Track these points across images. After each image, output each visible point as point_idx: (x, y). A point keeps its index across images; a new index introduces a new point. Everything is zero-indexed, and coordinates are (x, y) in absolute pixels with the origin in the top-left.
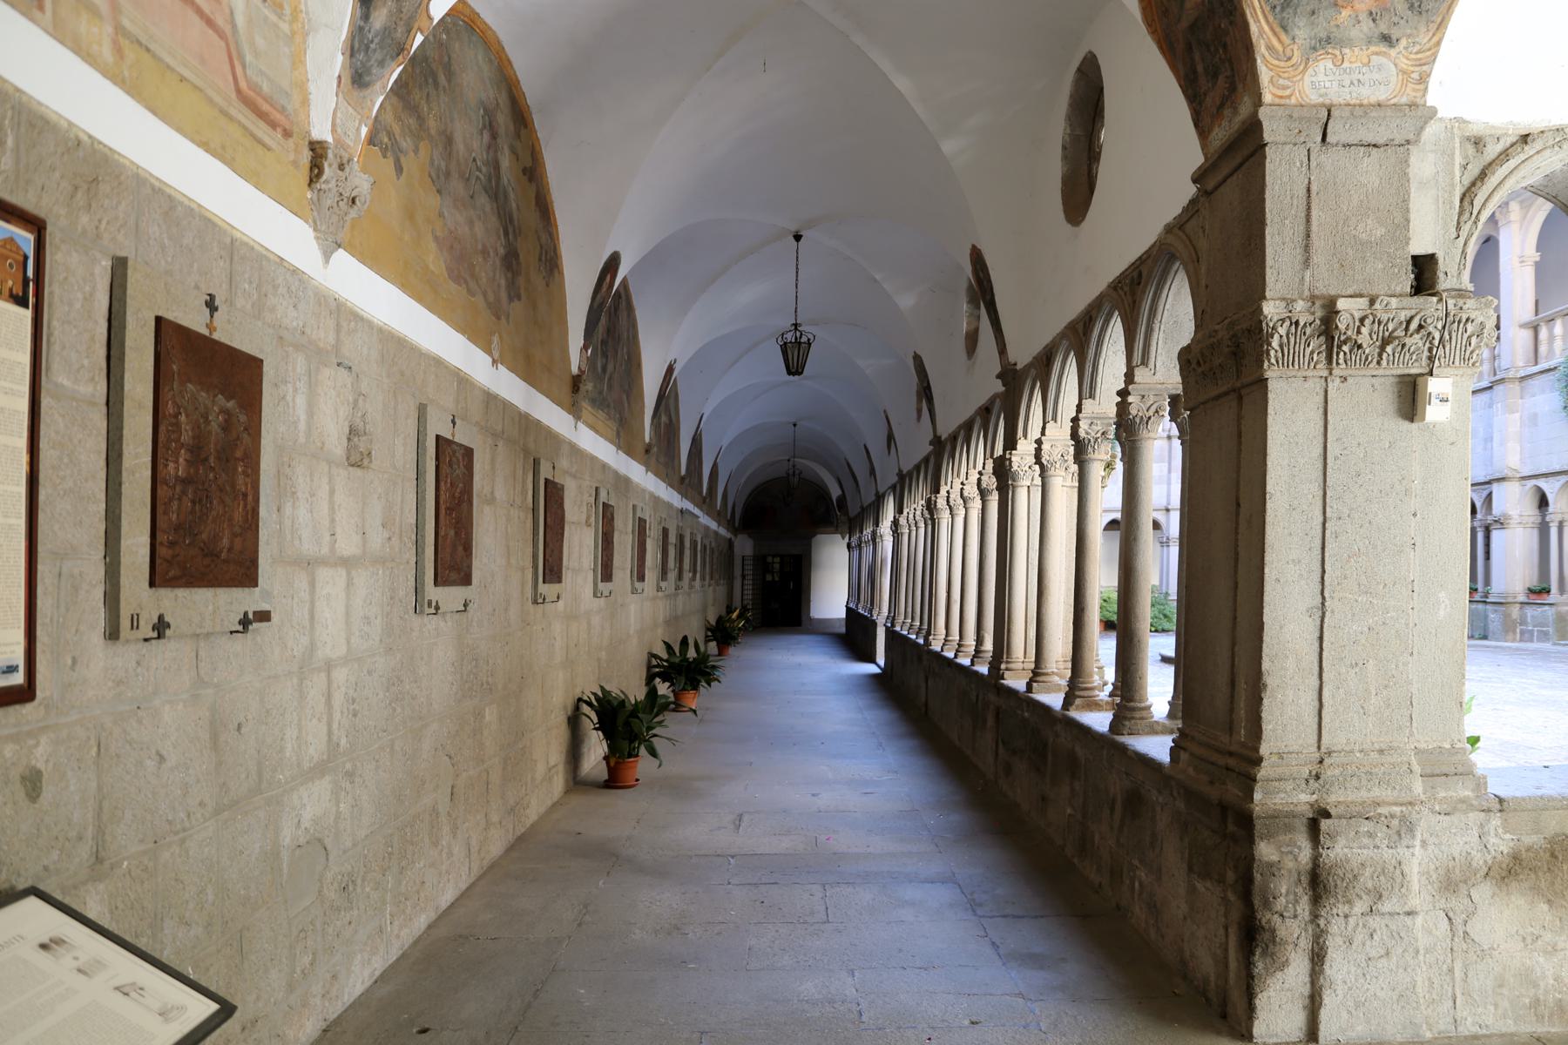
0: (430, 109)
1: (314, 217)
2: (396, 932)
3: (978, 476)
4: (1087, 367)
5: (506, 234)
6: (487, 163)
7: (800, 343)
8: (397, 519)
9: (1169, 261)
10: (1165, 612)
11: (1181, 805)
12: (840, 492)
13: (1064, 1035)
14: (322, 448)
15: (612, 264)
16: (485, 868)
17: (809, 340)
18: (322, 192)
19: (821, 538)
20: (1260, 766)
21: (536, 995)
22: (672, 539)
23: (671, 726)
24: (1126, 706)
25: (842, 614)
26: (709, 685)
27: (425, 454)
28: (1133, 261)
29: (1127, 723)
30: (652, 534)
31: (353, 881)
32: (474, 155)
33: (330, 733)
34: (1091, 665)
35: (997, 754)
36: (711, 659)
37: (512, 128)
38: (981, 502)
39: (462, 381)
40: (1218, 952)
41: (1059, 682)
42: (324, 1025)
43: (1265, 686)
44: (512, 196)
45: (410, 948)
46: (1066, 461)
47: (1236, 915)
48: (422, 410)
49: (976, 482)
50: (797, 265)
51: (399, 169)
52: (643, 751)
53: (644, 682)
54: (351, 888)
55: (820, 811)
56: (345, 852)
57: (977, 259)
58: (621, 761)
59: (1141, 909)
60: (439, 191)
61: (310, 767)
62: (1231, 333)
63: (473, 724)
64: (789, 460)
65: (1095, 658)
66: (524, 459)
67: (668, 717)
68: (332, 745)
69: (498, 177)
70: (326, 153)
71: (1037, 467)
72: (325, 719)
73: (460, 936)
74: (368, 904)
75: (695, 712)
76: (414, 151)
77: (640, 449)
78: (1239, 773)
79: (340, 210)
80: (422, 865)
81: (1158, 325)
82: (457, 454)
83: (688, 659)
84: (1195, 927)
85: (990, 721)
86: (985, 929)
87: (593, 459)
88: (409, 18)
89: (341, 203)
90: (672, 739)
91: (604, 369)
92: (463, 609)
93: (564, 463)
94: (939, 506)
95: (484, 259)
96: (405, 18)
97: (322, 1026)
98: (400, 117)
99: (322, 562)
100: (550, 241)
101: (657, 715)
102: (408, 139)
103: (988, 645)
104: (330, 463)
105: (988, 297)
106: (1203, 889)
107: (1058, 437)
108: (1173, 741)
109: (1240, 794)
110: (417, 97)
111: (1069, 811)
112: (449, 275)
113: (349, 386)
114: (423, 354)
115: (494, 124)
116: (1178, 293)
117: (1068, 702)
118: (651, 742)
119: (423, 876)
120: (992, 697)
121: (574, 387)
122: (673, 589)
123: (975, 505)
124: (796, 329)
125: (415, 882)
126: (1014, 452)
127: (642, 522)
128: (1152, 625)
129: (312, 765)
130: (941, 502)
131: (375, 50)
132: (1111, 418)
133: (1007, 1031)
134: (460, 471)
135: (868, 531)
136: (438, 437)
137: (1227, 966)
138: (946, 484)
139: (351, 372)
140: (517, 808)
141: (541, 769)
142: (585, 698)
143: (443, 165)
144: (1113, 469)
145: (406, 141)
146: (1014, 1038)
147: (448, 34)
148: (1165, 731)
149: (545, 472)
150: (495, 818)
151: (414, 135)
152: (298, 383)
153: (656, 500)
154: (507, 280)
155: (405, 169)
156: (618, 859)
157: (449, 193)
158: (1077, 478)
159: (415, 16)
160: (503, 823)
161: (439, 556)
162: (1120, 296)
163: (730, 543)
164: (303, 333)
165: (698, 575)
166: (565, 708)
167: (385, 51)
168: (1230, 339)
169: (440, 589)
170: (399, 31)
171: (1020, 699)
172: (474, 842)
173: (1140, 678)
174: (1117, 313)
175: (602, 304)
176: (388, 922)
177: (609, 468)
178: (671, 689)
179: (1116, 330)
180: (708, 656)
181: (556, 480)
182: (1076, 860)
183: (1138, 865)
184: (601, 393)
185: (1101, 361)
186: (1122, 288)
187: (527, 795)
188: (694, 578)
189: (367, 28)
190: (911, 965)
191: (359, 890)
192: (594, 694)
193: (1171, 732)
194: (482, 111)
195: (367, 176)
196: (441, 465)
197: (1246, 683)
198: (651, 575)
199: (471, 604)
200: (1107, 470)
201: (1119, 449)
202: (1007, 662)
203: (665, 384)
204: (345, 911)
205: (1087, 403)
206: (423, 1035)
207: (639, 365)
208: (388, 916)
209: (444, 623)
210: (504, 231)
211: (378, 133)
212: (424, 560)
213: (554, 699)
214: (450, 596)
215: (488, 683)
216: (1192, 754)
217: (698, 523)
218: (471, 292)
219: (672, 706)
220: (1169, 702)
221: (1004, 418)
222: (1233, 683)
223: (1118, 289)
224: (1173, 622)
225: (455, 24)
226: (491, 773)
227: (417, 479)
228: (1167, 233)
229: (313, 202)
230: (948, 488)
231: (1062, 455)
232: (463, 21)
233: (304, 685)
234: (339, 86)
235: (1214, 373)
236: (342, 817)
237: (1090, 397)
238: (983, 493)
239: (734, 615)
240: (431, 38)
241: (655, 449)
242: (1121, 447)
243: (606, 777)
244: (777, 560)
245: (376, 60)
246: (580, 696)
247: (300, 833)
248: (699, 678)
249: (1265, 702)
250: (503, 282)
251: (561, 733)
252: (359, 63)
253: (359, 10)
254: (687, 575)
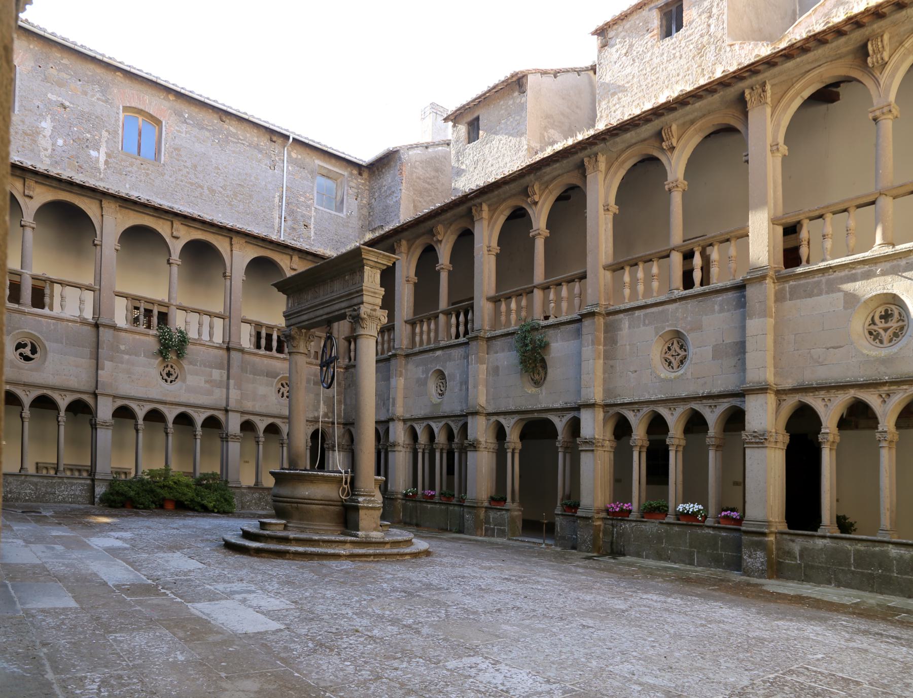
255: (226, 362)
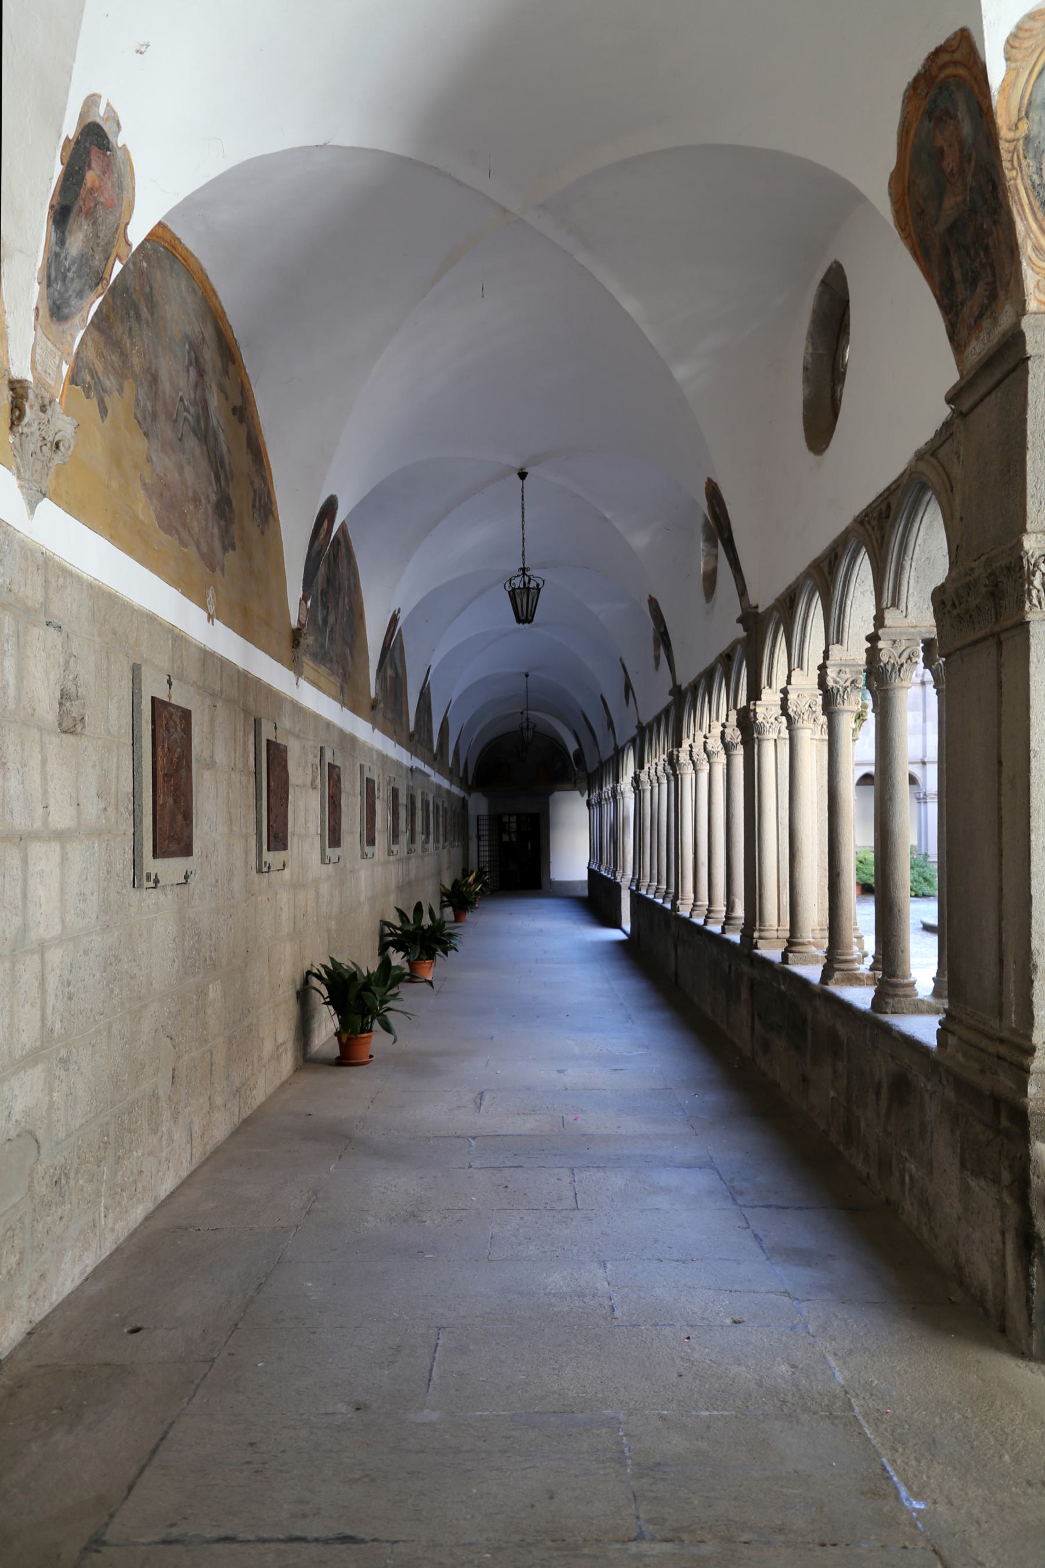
0: (133, 344)
1: (17, 464)
2: (110, 1226)
3: (722, 729)
4: (833, 609)
5: (218, 478)
6: (194, 403)
7: (529, 589)
8: (113, 789)
9: (920, 491)
10: (925, 875)
11: (950, 1094)
12: (577, 747)
13: (834, 1340)
14: (33, 715)
15: (329, 509)
16: (208, 1154)
17: (538, 585)
18: (24, 437)
19: (558, 795)
20: (1033, 1056)
21: (259, 1288)
22: (403, 799)
23: (407, 996)
24: (887, 982)
25: (584, 876)
26: (446, 954)
27: (140, 718)
28: (880, 492)
29: (890, 1000)
30: (381, 795)
31: (65, 1174)
32: (181, 394)
33: (43, 1018)
34: (849, 936)
35: (753, 1029)
36: (447, 925)
37: (219, 364)
38: (725, 756)
39: (177, 638)
40: (995, 1259)
41: (816, 953)
42: (28, 1327)
43: (1035, 967)
44: (222, 438)
45: (125, 1241)
46: (814, 712)
47: (1012, 1220)
48: (136, 671)
49: (720, 735)
50: (523, 505)
51: (103, 410)
52: (376, 1026)
53: (377, 952)
54: (63, 1181)
55: (566, 1089)
56: (58, 1144)
57: (713, 494)
58: (353, 1036)
59: (912, 1204)
60: (146, 434)
61: (22, 1056)
62: (989, 571)
63: (195, 1002)
64: (522, 713)
65: (853, 927)
66: (244, 720)
67: (403, 989)
68: (46, 1032)
69: (207, 418)
70: (27, 393)
71: (784, 719)
72: (39, 1004)
73: (179, 1228)
74: (80, 1197)
75: (431, 983)
76: (117, 390)
77: (366, 705)
78: (1011, 1063)
79: (44, 456)
80: (140, 1154)
81: (909, 562)
82: (174, 717)
83: (423, 926)
84: (971, 1229)
85: (745, 994)
86: (746, 1219)
87: (317, 717)
88: (106, 244)
89: (44, 448)
90: (407, 1013)
91: (325, 621)
92: (184, 881)
93: (286, 723)
94: (681, 760)
95: (196, 506)
96: (103, 243)
97: (26, 1328)
98: (102, 353)
99: (35, 836)
100: (263, 486)
101: (390, 988)
102: (111, 377)
103: (740, 911)
104: (41, 729)
105: (726, 535)
106: (977, 1189)
107: (805, 682)
108: (940, 1023)
109: (1013, 1086)
110: (119, 332)
111: (832, 1094)
112: (159, 526)
113: (59, 647)
114: (135, 610)
115: (201, 360)
116: (931, 526)
117: (827, 975)
118: (385, 1016)
119: (141, 1164)
120: (745, 968)
121: (294, 641)
122: (406, 852)
123: (719, 760)
124: (524, 574)
125: (132, 1173)
126: (758, 702)
127: (370, 783)
128: (911, 890)
129: (24, 1053)
130: (684, 757)
131: (73, 279)
132: (860, 665)
133: (772, 1332)
134: (177, 735)
135: (608, 788)
136: (154, 699)
137: (1005, 1275)
138: (688, 737)
139: (61, 631)
140: (243, 1089)
141: (268, 1047)
142: (315, 971)
143: (149, 404)
144: (864, 720)
145: (109, 379)
146: (780, 1340)
147: (148, 262)
148: (932, 1011)
149: (267, 732)
150: (219, 1100)
151: (118, 374)
152: (6, 645)
153: (384, 759)
154: (220, 527)
155: (109, 411)
156: (350, 1141)
157: (157, 436)
158: (827, 731)
159: (113, 242)
160: (229, 1105)
161: (158, 826)
162: (867, 531)
163: (464, 803)
164: (10, 591)
165: (431, 837)
166: (294, 982)
167: (83, 281)
168: (988, 578)
169: (159, 861)
170: (97, 258)
171: (776, 970)
172: (196, 1128)
173: (902, 952)
174: (865, 550)
175: (320, 552)
176: (103, 1215)
177: (334, 726)
178: (405, 959)
179: (864, 568)
180: (444, 922)
181: (279, 741)
182: (841, 1148)
183: (907, 1157)
184: (322, 646)
185: (849, 603)
186: (869, 522)
187: (253, 1075)
188: (427, 841)
189: (63, 255)
190: (667, 1257)
191: (72, 1183)
192: (324, 967)
193: (937, 1012)
194: (187, 346)
195: (70, 418)
196: (157, 728)
197: (1015, 962)
198: (382, 838)
199: (193, 876)
200: (858, 721)
201: (869, 697)
202: (761, 930)
203: (389, 636)
204: (56, 1205)
205: (834, 649)
206: (135, 1334)
207: (362, 616)
208: (102, 1209)
209: (164, 896)
210: (215, 477)
211: (80, 371)
212: (142, 831)
213: (282, 973)
214: (170, 868)
215: (211, 959)
216: (960, 1038)
217: (429, 781)
218: (183, 543)
219: (407, 977)
220: (933, 979)
221: (747, 666)
222: (1001, 962)
223: (865, 523)
224: (934, 887)
225: (155, 250)
226: (214, 1053)
227: (133, 745)
228: (917, 460)
229: (15, 448)
230: (691, 741)
231: (810, 706)
232: (164, 247)
233: (16, 969)
234: (37, 315)
235: (971, 616)
236: (55, 1107)
237: (838, 642)
238: (728, 747)
239: (471, 879)
240: (131, 266)
241: (382, 705)
242: (873, 696)
243: (337, 1052)
244: (514, 819)
245: (74, 291)
246: (309, 969)
247: (10, 1126)
248: (435, 946)
249: (1036, 984)
250: (216, 531)
251: (290, 1008)
252: (56, 293)
253: (53, 234)
254: (420, 838)
255: (920, 701)
